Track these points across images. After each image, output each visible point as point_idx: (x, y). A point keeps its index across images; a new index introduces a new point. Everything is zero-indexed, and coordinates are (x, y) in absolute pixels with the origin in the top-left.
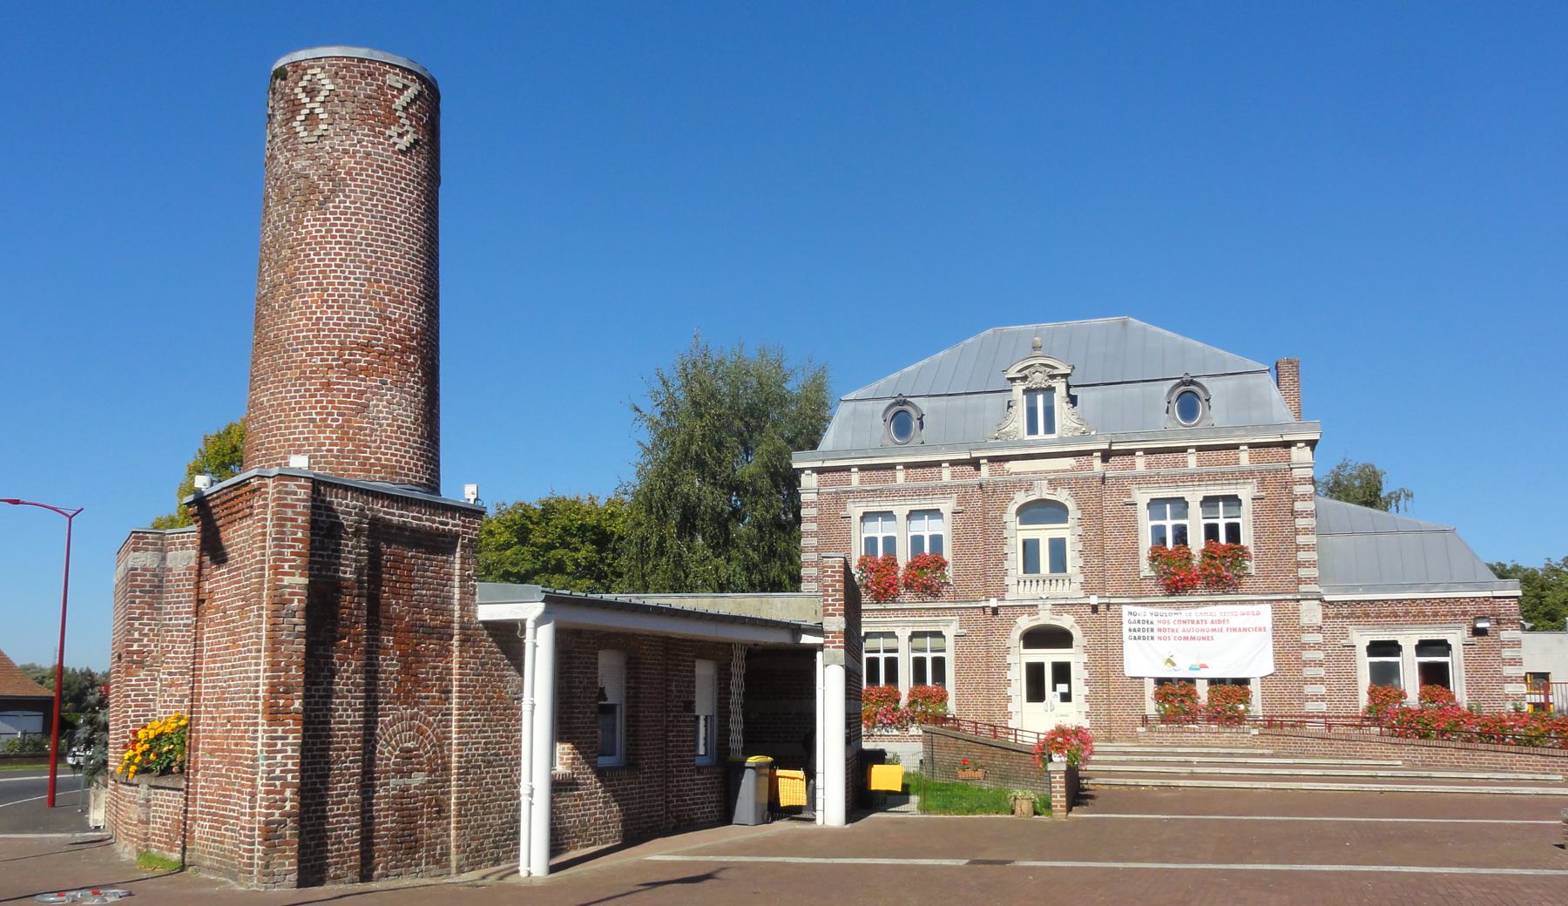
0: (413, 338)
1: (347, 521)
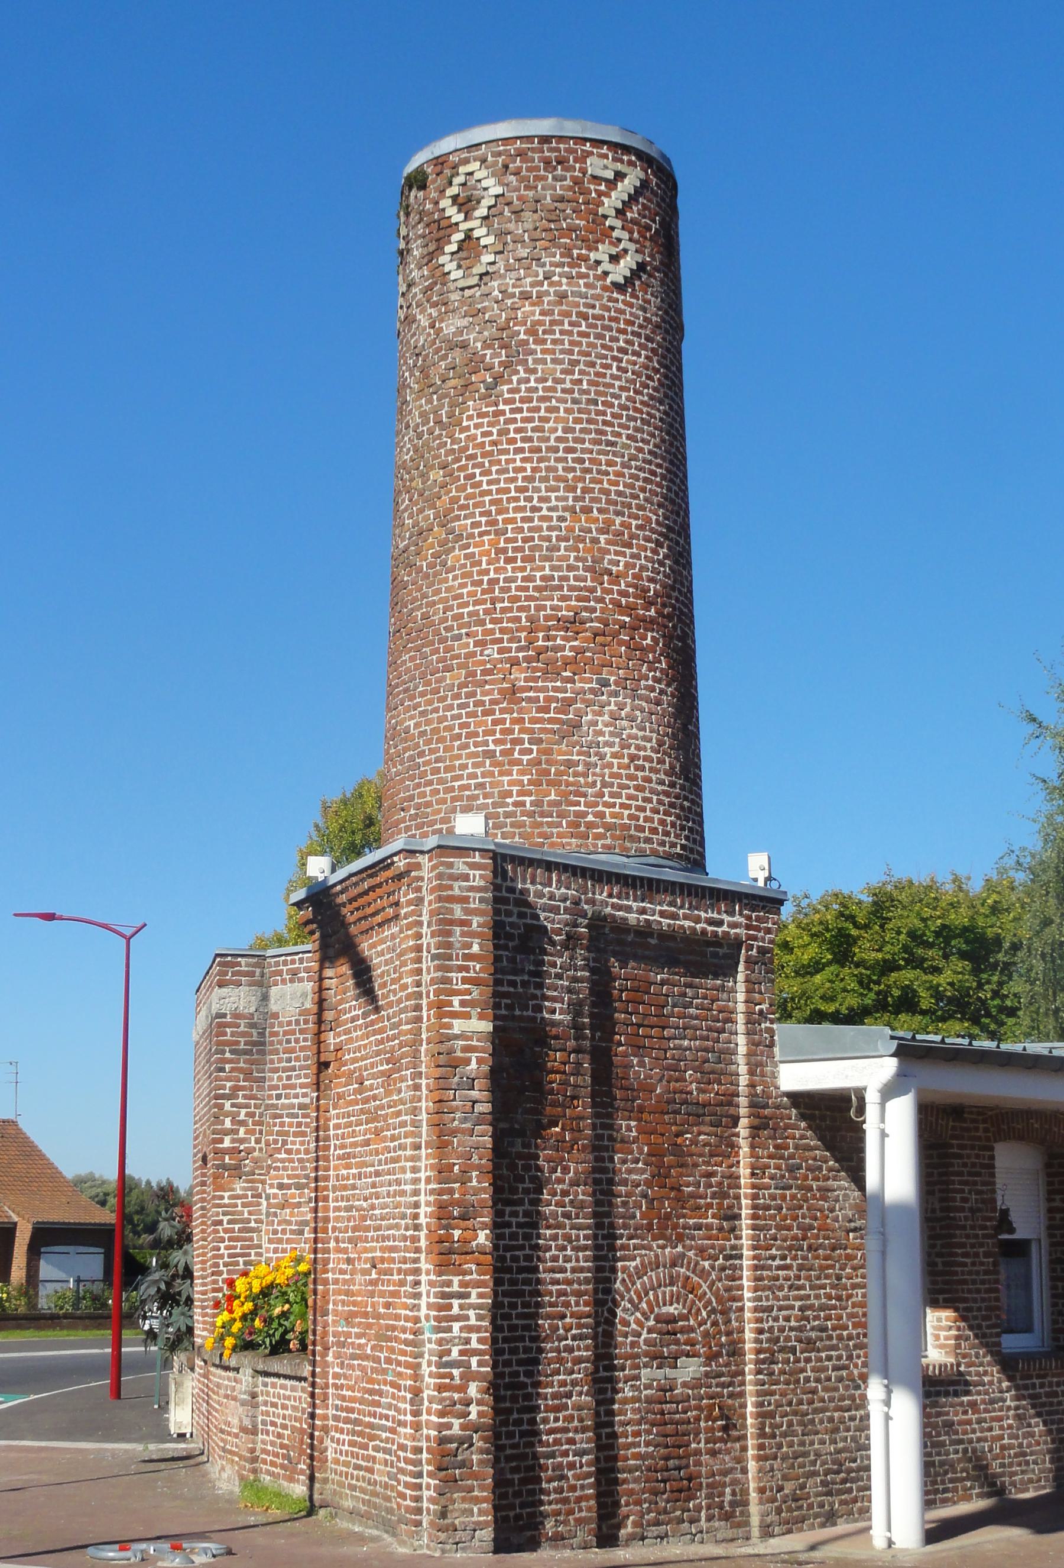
0: (649, 604)
1: (554, 922)
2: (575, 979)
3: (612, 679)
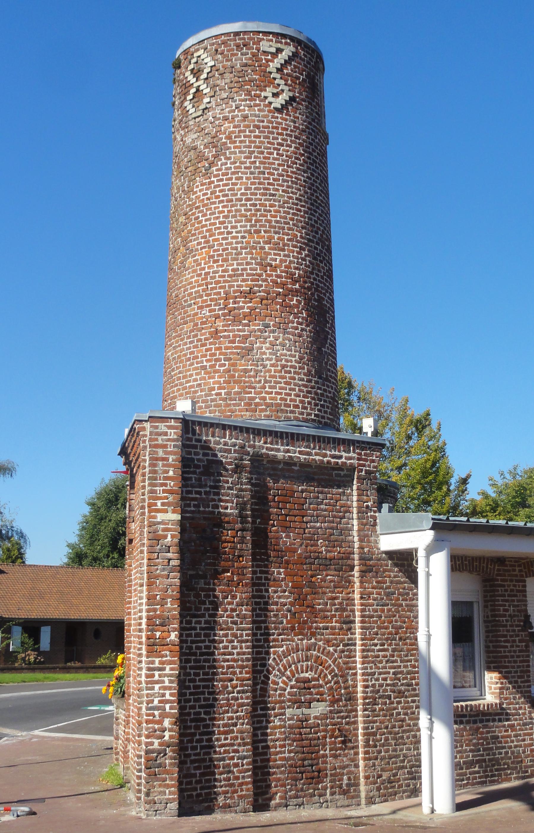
0: (295, 282)
1: (228, 459)
2: (241, 490)
3: (272, 323)
